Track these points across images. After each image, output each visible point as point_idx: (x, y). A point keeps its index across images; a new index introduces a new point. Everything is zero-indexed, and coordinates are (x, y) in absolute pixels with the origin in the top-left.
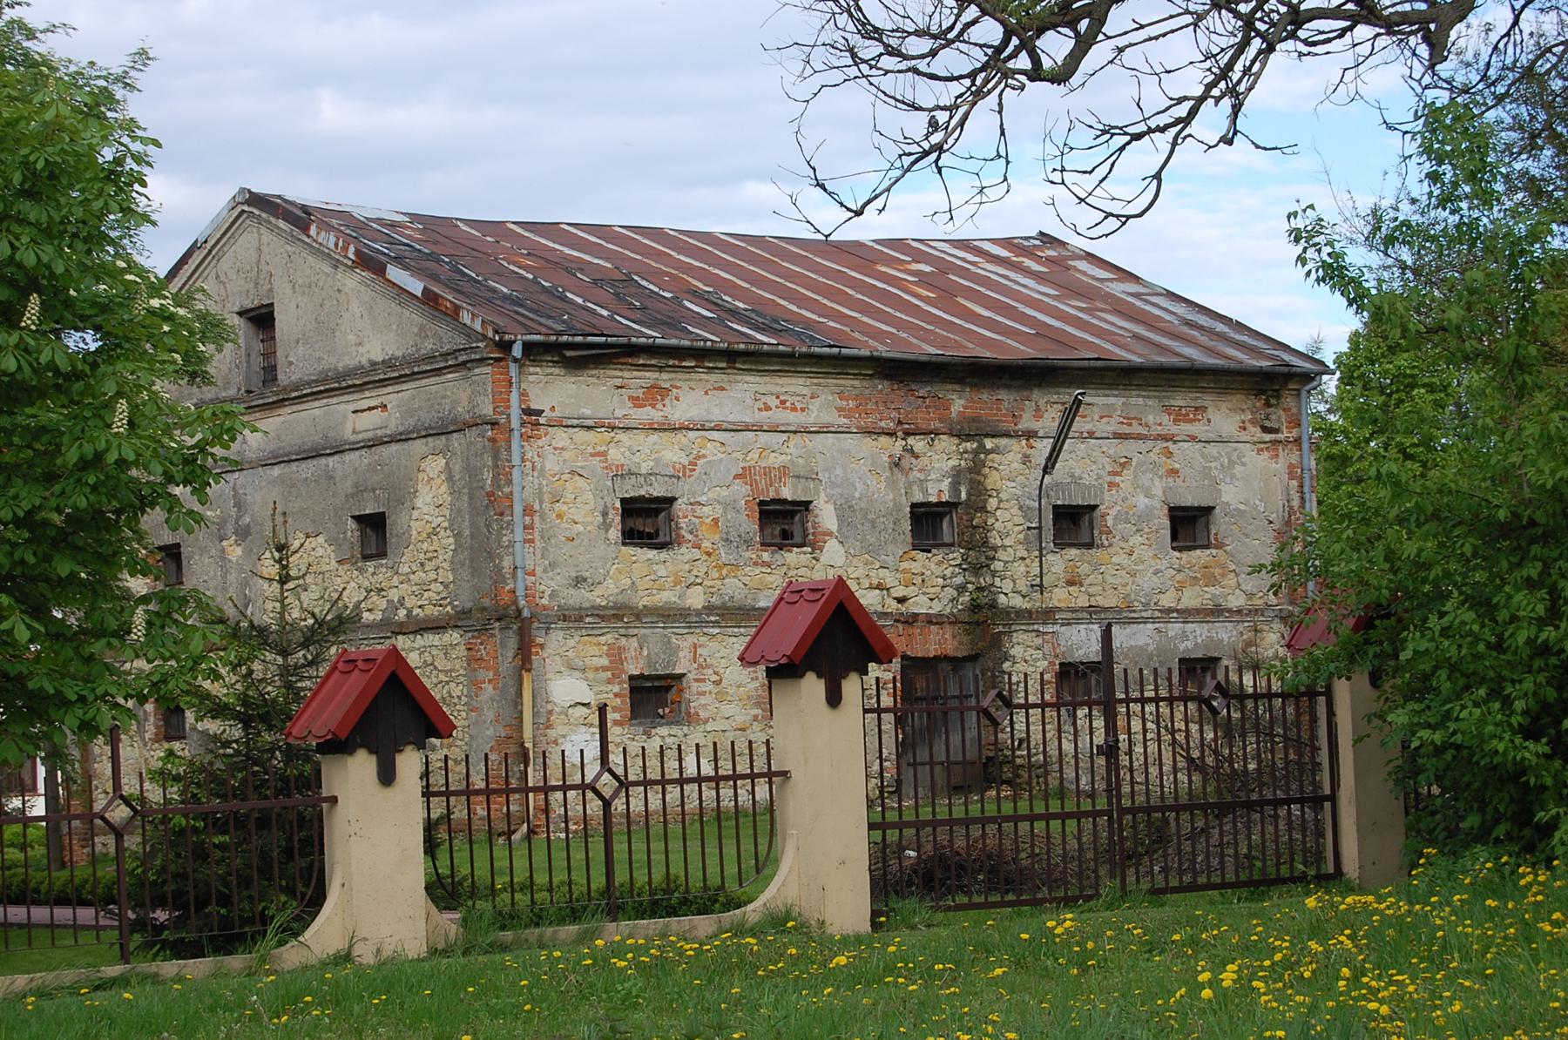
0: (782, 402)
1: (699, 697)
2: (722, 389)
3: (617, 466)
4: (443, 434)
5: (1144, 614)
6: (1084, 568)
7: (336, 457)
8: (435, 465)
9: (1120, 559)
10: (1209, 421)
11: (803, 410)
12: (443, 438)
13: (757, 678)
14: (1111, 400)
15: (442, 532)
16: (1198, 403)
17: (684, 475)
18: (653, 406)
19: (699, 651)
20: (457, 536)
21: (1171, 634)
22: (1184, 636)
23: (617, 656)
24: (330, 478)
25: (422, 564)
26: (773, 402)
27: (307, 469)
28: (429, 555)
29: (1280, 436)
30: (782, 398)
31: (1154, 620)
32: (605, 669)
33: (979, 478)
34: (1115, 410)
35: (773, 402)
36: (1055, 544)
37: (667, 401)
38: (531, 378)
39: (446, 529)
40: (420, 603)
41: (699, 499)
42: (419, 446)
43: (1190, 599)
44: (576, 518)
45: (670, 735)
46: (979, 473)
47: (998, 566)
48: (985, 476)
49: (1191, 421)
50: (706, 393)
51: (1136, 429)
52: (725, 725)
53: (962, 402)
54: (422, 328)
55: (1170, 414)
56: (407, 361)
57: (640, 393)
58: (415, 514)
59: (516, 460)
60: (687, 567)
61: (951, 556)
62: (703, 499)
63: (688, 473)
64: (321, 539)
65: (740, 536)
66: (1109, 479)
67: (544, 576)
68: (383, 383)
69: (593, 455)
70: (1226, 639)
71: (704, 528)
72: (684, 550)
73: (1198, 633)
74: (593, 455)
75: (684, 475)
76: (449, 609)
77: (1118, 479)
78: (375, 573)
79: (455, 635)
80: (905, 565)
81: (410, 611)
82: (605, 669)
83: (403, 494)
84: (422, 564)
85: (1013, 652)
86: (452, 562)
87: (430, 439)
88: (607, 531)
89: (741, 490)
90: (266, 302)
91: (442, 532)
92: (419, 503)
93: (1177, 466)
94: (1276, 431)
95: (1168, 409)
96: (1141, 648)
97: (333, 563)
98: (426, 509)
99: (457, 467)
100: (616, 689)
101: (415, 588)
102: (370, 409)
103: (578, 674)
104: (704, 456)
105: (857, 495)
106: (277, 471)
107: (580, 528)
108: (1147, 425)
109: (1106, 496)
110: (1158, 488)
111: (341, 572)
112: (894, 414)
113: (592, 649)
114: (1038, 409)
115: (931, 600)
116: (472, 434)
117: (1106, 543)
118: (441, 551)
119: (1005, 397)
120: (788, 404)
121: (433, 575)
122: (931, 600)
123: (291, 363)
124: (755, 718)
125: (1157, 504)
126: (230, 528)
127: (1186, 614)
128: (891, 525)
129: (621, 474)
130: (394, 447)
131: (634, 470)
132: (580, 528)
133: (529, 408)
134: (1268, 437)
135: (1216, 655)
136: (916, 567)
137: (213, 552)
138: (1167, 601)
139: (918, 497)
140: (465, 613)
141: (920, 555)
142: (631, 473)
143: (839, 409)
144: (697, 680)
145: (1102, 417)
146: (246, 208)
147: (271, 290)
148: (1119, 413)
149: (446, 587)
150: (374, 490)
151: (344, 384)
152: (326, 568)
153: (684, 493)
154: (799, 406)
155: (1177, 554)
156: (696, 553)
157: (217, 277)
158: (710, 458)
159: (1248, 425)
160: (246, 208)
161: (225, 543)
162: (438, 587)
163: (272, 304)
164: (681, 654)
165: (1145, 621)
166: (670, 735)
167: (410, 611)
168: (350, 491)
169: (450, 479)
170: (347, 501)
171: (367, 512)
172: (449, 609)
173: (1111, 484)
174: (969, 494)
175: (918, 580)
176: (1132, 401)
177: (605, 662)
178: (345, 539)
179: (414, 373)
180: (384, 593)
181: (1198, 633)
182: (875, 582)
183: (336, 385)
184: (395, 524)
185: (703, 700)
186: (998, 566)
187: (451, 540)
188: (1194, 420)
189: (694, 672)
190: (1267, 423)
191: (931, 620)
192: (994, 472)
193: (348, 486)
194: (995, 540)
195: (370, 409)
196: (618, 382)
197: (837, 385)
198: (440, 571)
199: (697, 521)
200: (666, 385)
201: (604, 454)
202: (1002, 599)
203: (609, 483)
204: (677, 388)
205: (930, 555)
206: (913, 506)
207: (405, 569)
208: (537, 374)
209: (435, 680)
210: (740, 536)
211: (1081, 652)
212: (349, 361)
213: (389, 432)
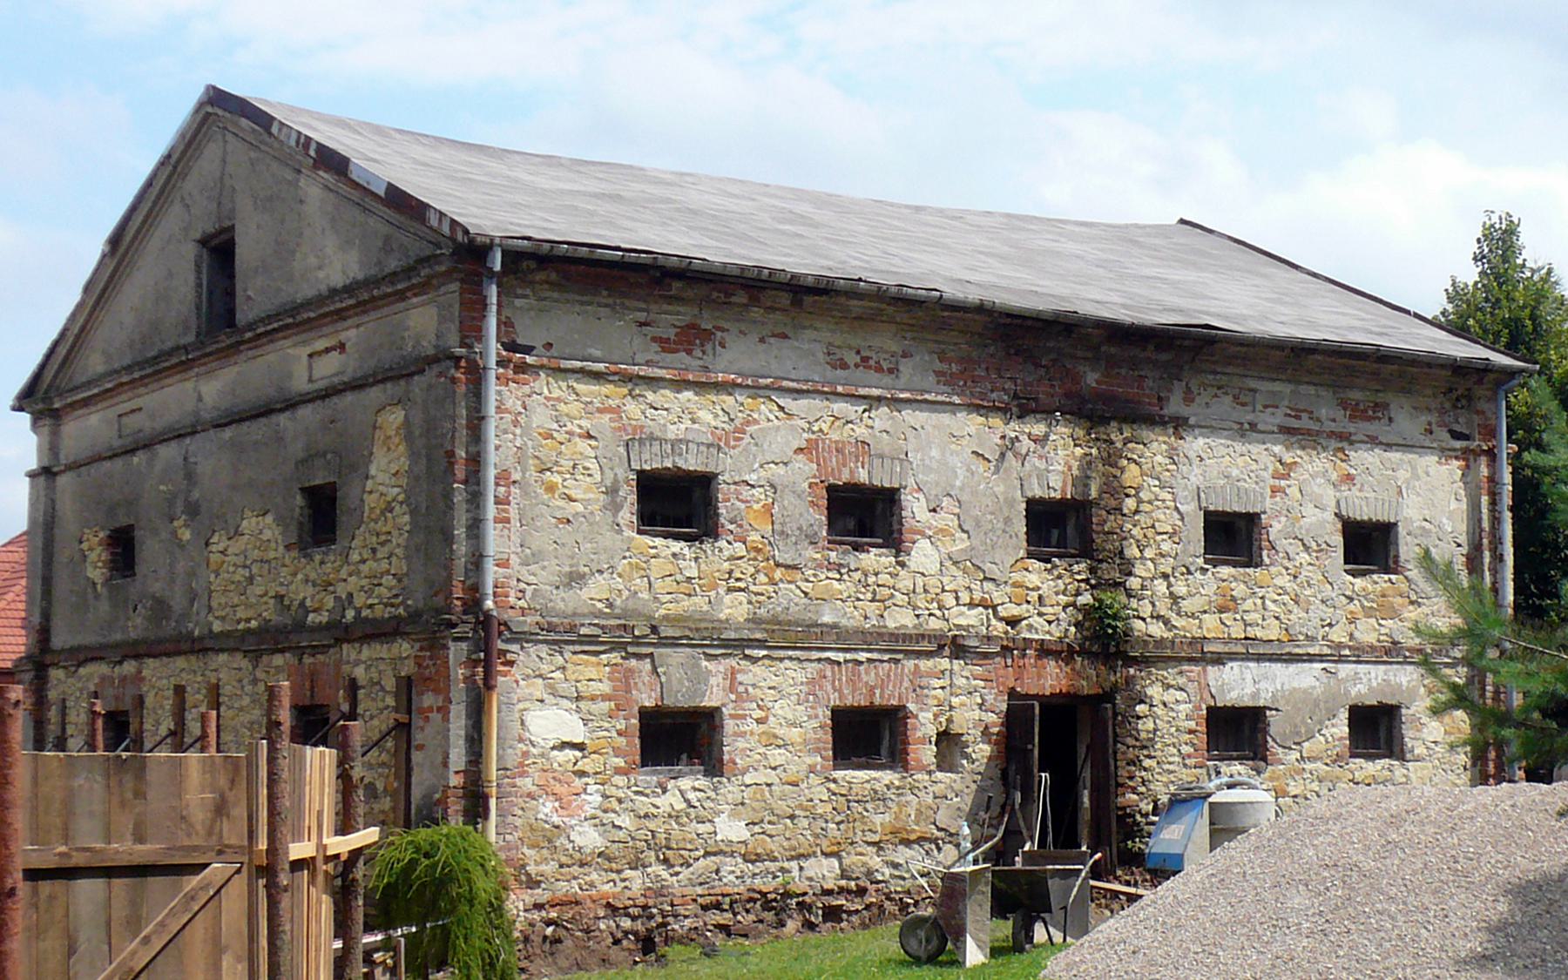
0: (865, 359)
1: (811, 725)
2: (785, 336)
3: (635, 428)
4: (403, 376)
5: (1311, 651)
6: (1239, 590)
7: (288, 414)
8: (394, 418)
9: (1284, 581)
10: (1390, 420)
11: (891, 371)
12: (402, 382)
13: (817, 716)
14: (1277, 387)
15: (397, 508)
16: (1381, 398)
17: (727, 444)
18: (689, 352)
19: (740, 677)
20: (413, 512)
21: (1341, 675)
22: (1356, 678)
23: (625, 681)
24: (280, 439)
25: (374, 551)
26: (852, 358)
27: (256, 430)
28: (383, 538)
29: (1474, 445)
30: (864, 354)
31: (1320, 658)
32: (606, 698)
33: (1113, 470)
34: (1283, 399)
35: (852, 358)
36: (1206, 562)
37: (708, 347)
38: (518, 302)
39: (402, 503)
40: (370, 601)
41: (747, 478)
42: (375, 394)
43: (1367, 633)
44: (572, 493)
45: (695, 789)
46: (1114, 465)
47: (1134, 583)
48: (1123, 470)
49: (1369, 419)
50: (762, 340)
51: (1305, 423)
52: (772, 776)
53: (1096, 376)
54: (387, 239)
55: (1345, 409)
56: (368, 283)
57: (671, 333)
58: (369, 485)
59: (491, 410)
60: (726, 565)
61: (1076, 568)
62: (752, 478)
63: (732, 443)
64: (269, 519)
65: (800, 529)
66: (1272, 482)
67: (524, 570)
68: (341, 315)
69: (600, 411)
70: (1405, 683)
71: (752, 515)
72: (722, 543)
73: (1373, 675)
74: (600, 411)
75: (727, 444)
76: (401, 610)
77: (1283, 483)
78: (324, 563)
79: (406, 645)
80: (1016, 577)
81: (358, 611)
82: (606, 698)
83: (354, 462)
84: (374, 551)
85: (1149, 691)
86: (406, 547)
87: (389, 385)
88: (615, 515)
89: (803, 472)
90: (227, 223)
91: (397, 508)
92: (373, 472)
93: (1353, 471)
94: (1466, 437)
95: (1344, 404)
96: (1305, 691)
97: (281, 548)
98: (381, 477)
99: (418, 418)
100: (621, 725)
101: (364, 582)
102: (327, 350)
103: (566, 703)
104: (756, 422)
105: (958, 483)
106: (228, 433)
107: (579, 507)
108: (1318, 420)
109: (1268, 502)
110: (1329, 496)
111: (287, 561)
112: (1009, 385)
113: (594, 673)
114: (1188, 390)
115: (1050, 623)
116: (430, 375)
117: (1267, 560)
118: (395, 533)
119: (1149, 374)
120: (872, 363)
121: (384, 565)
122: (1050, 623)
123: (249, 298)
124: (812, 769)
125: (1329, 516)
126: (179, 506)
127: (1361, 653)
128: (1001, 525)
129: (636, 439)
130: (349, 398)
131: (658, 433)
132: (579, 507)
133: (514, 342)
134: (1458, 444)
135: (1394, 702)
136: (1033, 579)
137: (164, 535)
138: (1338, 635)
139: (1037, 492)
140: (414, 616)
141: (1036, 565)
142: (652, 438)
143: (938, 373)
144: (732, 716)
145: (1266, 407)
146: (210, 109)
147: (233, 210)
148: (1286, 403)
149: (400, 581)
150: (324, 454)
151: (299, 318)
152: (272, 555)
153: (727, 467)
154: (885, 365)
155: (1350, 578)
156: (739, 548)
157: (183, 199)
158: (764, 424)
159: (1434, 427)
160: (210, 109)
161: (176, 523)
162: (388, 580)
163: (233, 226)
164: (713, 681)
165: (1311, 658)
166: (695, 789)
167: (358, 611)
168: (301, 455)
169: (409, 438)
170: (297, 468)
171: (317, 482)
172: (401, 610)
173: (1275, 490)
174: (1101, 492)
175: (1034, 596)
176: (1303, 388)
177: (605, 687)
178: (292, 518)
179: (373, 299)
180: (331, 588)
181: (1373, 675)
182: (977, 596)
183: (290, 320)
184: (348, 496)
185: (741, 744)
186: (1134, 583)
187: (407, 518)
188: (1375, 418)
189: (731, 705)
190: (1457, 428)
191: (1044, 651)
192: (1133, 466)
193: (297, 449)
194: (1132, 551)
195: (327, 350)
196: (642, 316)
197: (936, 342)
198: (394, 559)
199: (743, 506)
200: (709, 327)
201: (617, 410)
202: (1138, 624)
203: (622, 450)
204: (723, 330)
205: (1049, 566)
206: (1031, 503)
207: (355, 557)
208: (525, 296)
209: (381, 705)
210: (800, 529)
211: (1234, 694)
212: (307, 292)
213: (346, 379)
